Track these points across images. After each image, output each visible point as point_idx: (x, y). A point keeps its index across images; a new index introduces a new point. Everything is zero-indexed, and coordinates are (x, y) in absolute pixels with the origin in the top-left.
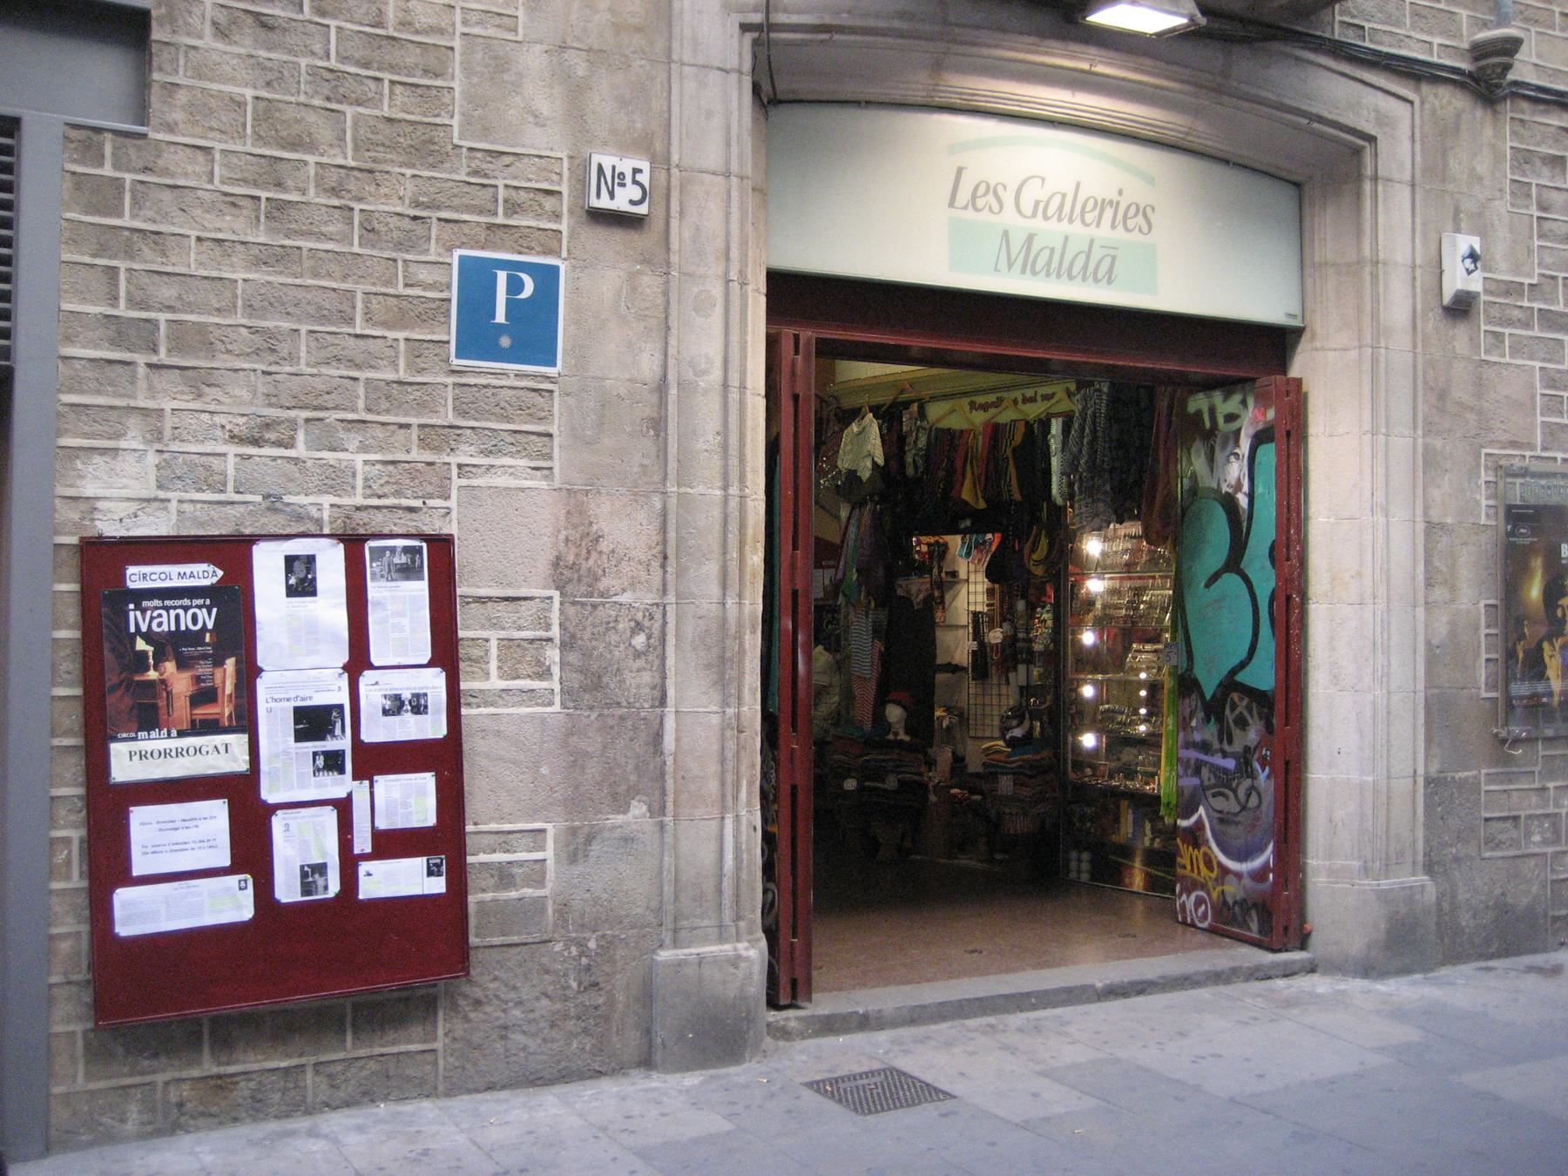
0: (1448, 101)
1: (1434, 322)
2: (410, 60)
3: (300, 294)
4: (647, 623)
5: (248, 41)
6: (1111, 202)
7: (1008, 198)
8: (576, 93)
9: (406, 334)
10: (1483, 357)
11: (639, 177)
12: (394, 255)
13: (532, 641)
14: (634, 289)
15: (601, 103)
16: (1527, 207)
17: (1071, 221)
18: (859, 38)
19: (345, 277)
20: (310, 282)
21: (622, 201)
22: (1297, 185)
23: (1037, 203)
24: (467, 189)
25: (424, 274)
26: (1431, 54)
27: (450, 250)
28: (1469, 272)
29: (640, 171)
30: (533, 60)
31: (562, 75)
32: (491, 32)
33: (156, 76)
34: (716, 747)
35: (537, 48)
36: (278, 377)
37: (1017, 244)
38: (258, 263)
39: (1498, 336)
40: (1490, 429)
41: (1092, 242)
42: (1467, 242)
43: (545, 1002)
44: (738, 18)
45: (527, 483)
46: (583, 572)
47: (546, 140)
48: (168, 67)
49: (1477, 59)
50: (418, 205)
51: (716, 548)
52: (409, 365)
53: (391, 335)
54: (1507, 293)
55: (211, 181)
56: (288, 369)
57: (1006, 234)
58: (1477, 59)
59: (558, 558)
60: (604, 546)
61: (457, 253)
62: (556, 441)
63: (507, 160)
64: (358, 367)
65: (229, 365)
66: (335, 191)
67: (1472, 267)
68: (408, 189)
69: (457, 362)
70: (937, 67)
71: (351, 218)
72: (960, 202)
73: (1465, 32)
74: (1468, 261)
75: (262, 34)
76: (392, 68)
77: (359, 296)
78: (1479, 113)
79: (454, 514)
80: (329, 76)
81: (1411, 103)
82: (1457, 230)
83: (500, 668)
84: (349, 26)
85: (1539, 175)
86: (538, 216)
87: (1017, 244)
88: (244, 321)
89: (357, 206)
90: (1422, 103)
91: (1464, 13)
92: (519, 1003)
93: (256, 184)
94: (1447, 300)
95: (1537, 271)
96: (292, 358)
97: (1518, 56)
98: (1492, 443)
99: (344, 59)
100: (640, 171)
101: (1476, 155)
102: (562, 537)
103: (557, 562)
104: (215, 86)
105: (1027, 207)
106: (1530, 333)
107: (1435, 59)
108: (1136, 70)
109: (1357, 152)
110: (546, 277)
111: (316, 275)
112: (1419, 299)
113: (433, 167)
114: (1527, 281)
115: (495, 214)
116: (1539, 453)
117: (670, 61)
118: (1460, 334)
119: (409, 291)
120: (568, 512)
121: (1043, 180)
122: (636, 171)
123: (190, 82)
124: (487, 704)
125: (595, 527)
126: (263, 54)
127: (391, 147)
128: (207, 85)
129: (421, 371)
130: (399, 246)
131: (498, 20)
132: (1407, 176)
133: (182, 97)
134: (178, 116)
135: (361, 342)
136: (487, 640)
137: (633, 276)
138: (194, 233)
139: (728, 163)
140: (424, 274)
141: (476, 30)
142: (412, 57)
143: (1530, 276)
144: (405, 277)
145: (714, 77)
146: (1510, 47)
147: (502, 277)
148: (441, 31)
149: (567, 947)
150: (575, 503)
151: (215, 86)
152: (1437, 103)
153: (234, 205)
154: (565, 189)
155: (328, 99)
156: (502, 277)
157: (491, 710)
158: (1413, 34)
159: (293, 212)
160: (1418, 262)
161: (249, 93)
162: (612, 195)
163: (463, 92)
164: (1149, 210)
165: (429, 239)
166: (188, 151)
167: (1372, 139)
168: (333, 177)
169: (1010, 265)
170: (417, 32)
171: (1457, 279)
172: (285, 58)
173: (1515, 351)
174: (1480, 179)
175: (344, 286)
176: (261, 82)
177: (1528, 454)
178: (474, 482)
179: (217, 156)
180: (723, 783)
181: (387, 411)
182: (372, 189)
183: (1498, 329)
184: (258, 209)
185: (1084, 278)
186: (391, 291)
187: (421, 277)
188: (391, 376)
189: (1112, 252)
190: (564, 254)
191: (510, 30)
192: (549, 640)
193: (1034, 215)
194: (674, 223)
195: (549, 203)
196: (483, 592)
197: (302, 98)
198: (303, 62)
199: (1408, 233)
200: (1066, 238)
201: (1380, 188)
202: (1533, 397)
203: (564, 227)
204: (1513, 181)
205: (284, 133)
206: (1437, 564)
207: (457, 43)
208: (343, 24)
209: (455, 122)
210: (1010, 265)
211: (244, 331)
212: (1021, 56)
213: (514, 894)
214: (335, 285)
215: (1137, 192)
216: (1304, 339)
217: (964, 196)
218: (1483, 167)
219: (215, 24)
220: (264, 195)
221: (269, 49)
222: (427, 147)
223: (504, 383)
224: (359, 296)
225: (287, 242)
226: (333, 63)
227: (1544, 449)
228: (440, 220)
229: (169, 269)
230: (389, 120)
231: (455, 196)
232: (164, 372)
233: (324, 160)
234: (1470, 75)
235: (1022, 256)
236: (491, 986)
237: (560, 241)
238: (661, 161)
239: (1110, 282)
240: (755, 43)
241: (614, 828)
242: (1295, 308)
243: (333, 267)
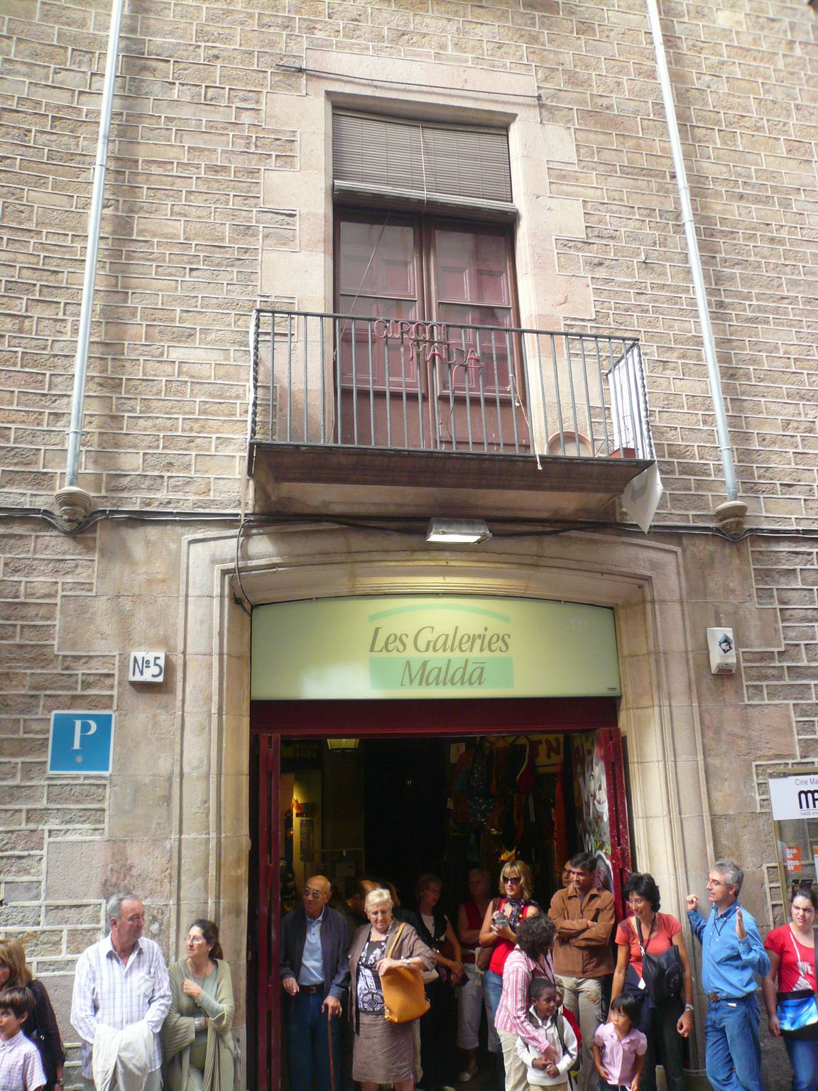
0: (703, 548)
4: (160, 917)
6: (479, 636)
7: (409, 642)
9: (23, 759)
10: (747, 702)
11: (158, 662)
13: (88, 931)
14: (155, 723)
16: (771, 604)
17: (452, 650)
21: (149, 675)
22: (611, 608)
23: (429, 643)
25: (35, 726)
26: (689, 521)
27: (50, 711)
28: (725, 651)
29: (159, 658)
30: (101, 605)
32: (78, 593)
37: (415, 668)
39: (758, 688)
40: (758, 749)
41: (467, 661)
45: (88, 838)
46: (121, 888)
53: (14, 760)
54: (762, 659)
57: (408, 663)
58: (721, 520)
59: (106, 881)
60: (135, 872)
62: (107, 813)
67: (728, 648)
68: (28, 681)
69: (50, 773)
70: (353, 576)
72: (377, 647)
73: (711, 506)
74: (724, 646)
78: (727, 551)
79: (45, 859)
81: (676, 552)
82: (719, 625)
83: (68, 947)
85: (778, 583)
87: (415, 668)
90: (684, 551)
94: (714, 669)
95: (784, 642)
98: (759, 758)
100: (159, 658)
101: (728, 577)
102: (109, 868)
103: (105, 884)
105: (422, 645)
106: (782, 683)
107: (691, 524)
110: (104, 722)
112: (692, 672)
114: (776, 650)
115: (76, 689)
116: (798, 760)
119: (27, 736)
120: (113, 853)
121: (433, 628)
124: (58, 969)
125: (129, 862)
130: (22, 712)
132: (677, 597)
136: (62, 931)
140: (35, 726)
143: (779, 646)
144: (24, 728)
147: (78, 724)
150: (117, 846)
152: (695, 550)
156: (78, 724)
157: (62, 973)
158: (674, 511)
160: (690, 649)
162: (142, 673)
164: (506, 637)
169: (411, 681)
170: (38, 598)
171: (717, 658)
173: (771, 696)
174: (733, 591)
177: (790, 761)
178: (59, 839)
181: (9, 803)
183: (758, 683)
185: (462, 684)
187: (33, 727)
189: (481, 665)
190: (115, 708)
191: (88, 591)
192: (99, 929)
193: (427, 649)
196: (59, 902)
199: (680, 631)
200: (449, 661)
201: (657, 607)
202: (790, 724)
204: (757, 589)
206: (724, 842)
210: (411, 681)
215: (496, 627)
216: (623, 705)
217: (380, 643)
223: (77, 782)
227: (802, 757)
228: (46, 695)
231: (55, 682)
234: (717, 529)
235: (419, 677)
237: (112, 701)
239: (480, 683)
242: (616, 685)
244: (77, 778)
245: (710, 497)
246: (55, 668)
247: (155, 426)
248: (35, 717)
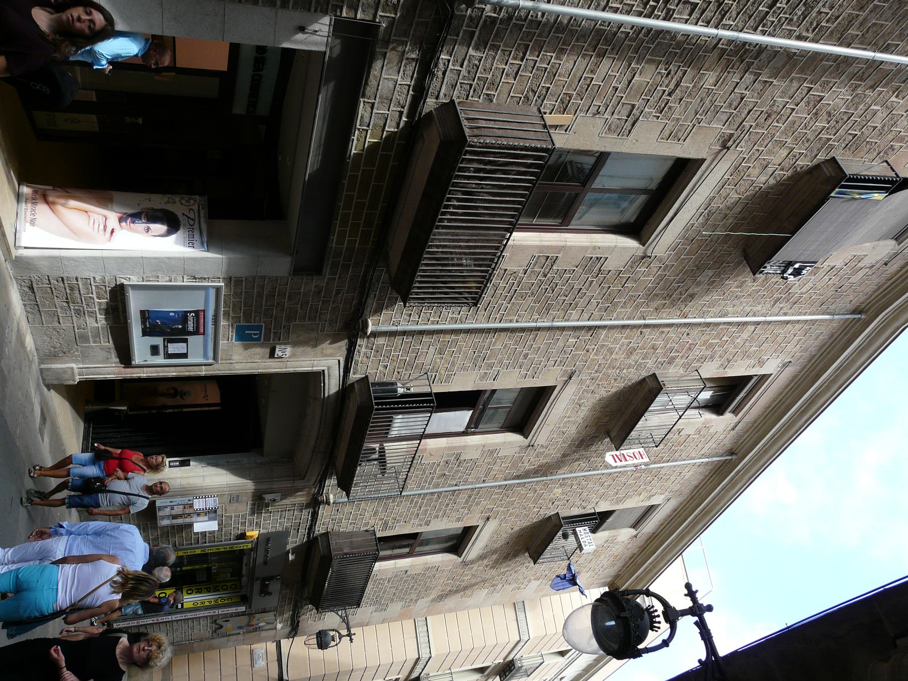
25: (257, 318)
66: (278, 304)
222: (289, 318)
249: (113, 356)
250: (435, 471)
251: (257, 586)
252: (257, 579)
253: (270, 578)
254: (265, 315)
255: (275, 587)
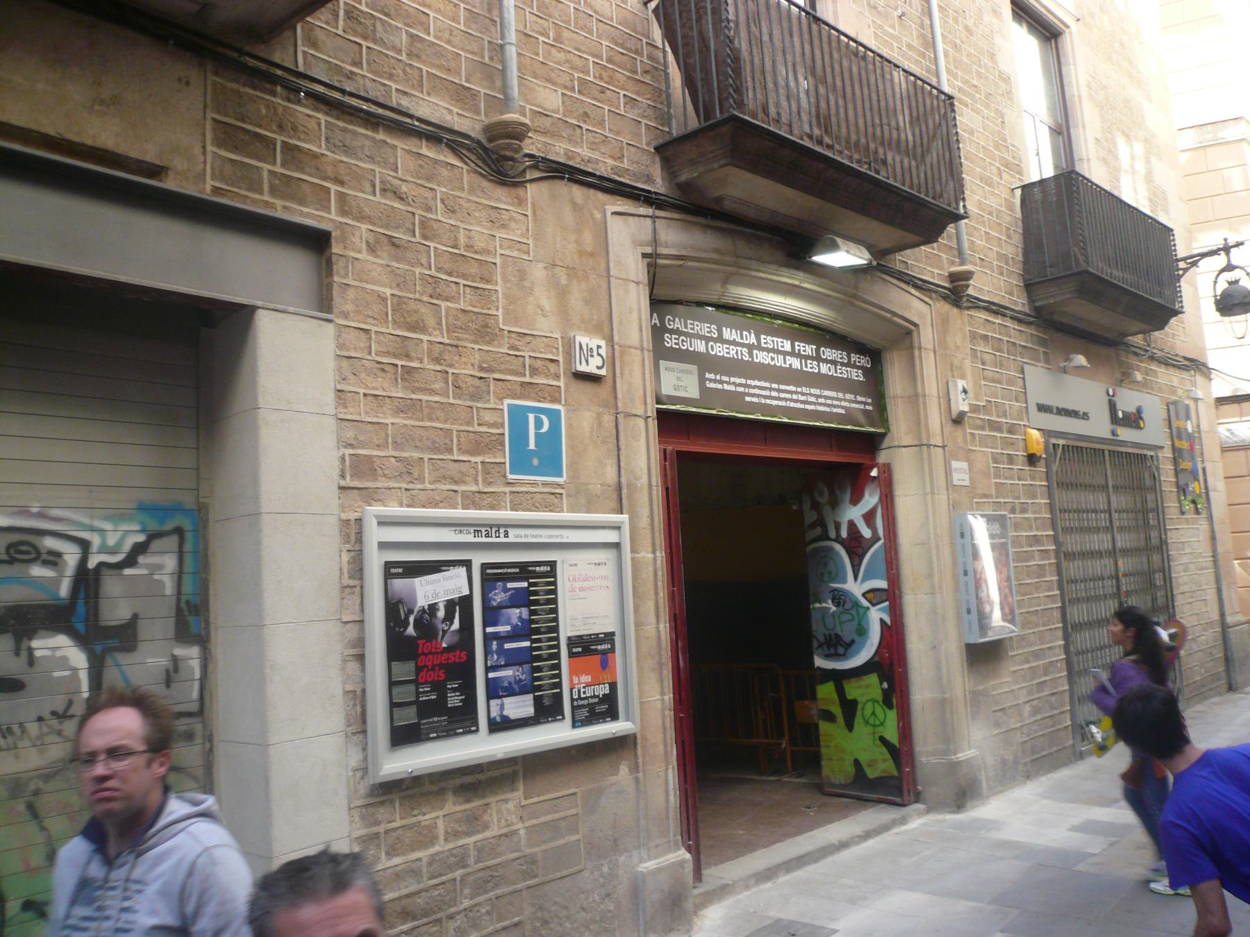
1: (949, 427)
2: (473, 271)
3: (424, 433)
5: (385, 255)
8: (562, 294)
11: (601, 351)
12: (471, 404)
14: (600, 424)
15: (576, 300)
18: (696, 264)
19: (446, 421)
20: (428, 424)
21: (592, 366)
24: (508, 358)
25: (488, 417)
27: (501, 399)
30: (538, 273)
31: (554, 283)
32: (515, 254)
33: (336, 278)
34: (660, 722)
35: (541, 265)
36: (414, 492)
38: (399, 411)
42: (961, 384)
43: (583, 914)
44: (641, 250)
47: (547, 326)
48: (342, 272)
49: (952, 282)
50: (482, 369)
51: (652, 593)
52: (484, 480)
53: (473, 459)
55: (370, 353)
56: (419, 486)
61: (507, 401)
63: (529, 339)
64: (456, 483)
65: (386, 485)
66: (437, 361)
69: (510, 476)
70: (726, 281)
71: (447, 379)
75: (393, 250)
76: (464, 276)
77: (455, 433)
80: (430, 280)
84: (440, 246)
86: (547, 376)
88: (393, 453)
89: (451, 371)
91: (944, 256)
92: (568, 918)
93: (395, 356)
96: (421, 479)
97: (971, 282)
99: (439, 269)
104: (369, 286)
108: (819, 286)
109: (909, 333)
110: (554, 416)
111: (431, 419)
113: (489, 343)
117: (609, 276)
118: (959, 433)
122: (599, 347)
123: (356, 283)
126: (395, 264)
127: (465, 329)
128: (364, 285)
129: (490, 484)
131: (518, 246)
133: (351, 294)
134: (349, 307)
135: (456, 465)
137: (599, 416)
138: (362, 391)
139: (641, 341)
141: (507, 252)
142: (474, 269)
145: (632, 286)
146: (967, 276)
148: (488, 252)
149: (592, 873)
151: (369, 286)
153: (383, 370)
154: (560, 359)
155: (431, 296)
156: (531, 417)
159: (416, 375)
161: (388, 292)
163: (504, 294)
165: (489, 393)
166: (356, 332)
167: (916, 325)
168: (437, 348)
170: (476, 252)
172: (407, 267)
175: (447, 426)
176: (394, 285)
179: (373, 336)
180: (665, 746)
182: (457, 358)
184: (396, 373)
186: (471, 429)
188: (475, 488)
194: (618, 380)
195: (552, 367)
197: (417, 296)
198: (418, 270)
203: (562, 384)
205: (408, 320)
207: (498, 260)
208: (440, 246)
209: (500, 313)
211: (393, 460)
212: (770, 277)
213: (562, 842)
214: (441, 426)
218: (959, 342)
219: (367, 243)
220: (400, 363)
221: (397, 261)
222: (486, 332)
224: (455, 433)
225: (413, 396)
226: (433, 272)
229: (349, 417)
230: (464, 311)
232: (348, 492)
233: (431, 339)
236: (553, 909)
238: (610, 340)
240: (649, 265)
241: (611, 785)
243: (439, 413)
244: (535, 484)
245: (265, 175)
246: (500, 346)
247: (567, 61)
248: (488, 406)
249: (613, 779)
250: (893, 37)
251: (1125, 434)
252: (1114, 433)
253: (1112, 407)
254: (476, 397)
255: (1128, 401)
